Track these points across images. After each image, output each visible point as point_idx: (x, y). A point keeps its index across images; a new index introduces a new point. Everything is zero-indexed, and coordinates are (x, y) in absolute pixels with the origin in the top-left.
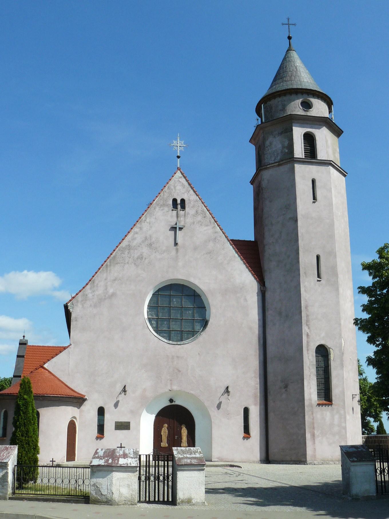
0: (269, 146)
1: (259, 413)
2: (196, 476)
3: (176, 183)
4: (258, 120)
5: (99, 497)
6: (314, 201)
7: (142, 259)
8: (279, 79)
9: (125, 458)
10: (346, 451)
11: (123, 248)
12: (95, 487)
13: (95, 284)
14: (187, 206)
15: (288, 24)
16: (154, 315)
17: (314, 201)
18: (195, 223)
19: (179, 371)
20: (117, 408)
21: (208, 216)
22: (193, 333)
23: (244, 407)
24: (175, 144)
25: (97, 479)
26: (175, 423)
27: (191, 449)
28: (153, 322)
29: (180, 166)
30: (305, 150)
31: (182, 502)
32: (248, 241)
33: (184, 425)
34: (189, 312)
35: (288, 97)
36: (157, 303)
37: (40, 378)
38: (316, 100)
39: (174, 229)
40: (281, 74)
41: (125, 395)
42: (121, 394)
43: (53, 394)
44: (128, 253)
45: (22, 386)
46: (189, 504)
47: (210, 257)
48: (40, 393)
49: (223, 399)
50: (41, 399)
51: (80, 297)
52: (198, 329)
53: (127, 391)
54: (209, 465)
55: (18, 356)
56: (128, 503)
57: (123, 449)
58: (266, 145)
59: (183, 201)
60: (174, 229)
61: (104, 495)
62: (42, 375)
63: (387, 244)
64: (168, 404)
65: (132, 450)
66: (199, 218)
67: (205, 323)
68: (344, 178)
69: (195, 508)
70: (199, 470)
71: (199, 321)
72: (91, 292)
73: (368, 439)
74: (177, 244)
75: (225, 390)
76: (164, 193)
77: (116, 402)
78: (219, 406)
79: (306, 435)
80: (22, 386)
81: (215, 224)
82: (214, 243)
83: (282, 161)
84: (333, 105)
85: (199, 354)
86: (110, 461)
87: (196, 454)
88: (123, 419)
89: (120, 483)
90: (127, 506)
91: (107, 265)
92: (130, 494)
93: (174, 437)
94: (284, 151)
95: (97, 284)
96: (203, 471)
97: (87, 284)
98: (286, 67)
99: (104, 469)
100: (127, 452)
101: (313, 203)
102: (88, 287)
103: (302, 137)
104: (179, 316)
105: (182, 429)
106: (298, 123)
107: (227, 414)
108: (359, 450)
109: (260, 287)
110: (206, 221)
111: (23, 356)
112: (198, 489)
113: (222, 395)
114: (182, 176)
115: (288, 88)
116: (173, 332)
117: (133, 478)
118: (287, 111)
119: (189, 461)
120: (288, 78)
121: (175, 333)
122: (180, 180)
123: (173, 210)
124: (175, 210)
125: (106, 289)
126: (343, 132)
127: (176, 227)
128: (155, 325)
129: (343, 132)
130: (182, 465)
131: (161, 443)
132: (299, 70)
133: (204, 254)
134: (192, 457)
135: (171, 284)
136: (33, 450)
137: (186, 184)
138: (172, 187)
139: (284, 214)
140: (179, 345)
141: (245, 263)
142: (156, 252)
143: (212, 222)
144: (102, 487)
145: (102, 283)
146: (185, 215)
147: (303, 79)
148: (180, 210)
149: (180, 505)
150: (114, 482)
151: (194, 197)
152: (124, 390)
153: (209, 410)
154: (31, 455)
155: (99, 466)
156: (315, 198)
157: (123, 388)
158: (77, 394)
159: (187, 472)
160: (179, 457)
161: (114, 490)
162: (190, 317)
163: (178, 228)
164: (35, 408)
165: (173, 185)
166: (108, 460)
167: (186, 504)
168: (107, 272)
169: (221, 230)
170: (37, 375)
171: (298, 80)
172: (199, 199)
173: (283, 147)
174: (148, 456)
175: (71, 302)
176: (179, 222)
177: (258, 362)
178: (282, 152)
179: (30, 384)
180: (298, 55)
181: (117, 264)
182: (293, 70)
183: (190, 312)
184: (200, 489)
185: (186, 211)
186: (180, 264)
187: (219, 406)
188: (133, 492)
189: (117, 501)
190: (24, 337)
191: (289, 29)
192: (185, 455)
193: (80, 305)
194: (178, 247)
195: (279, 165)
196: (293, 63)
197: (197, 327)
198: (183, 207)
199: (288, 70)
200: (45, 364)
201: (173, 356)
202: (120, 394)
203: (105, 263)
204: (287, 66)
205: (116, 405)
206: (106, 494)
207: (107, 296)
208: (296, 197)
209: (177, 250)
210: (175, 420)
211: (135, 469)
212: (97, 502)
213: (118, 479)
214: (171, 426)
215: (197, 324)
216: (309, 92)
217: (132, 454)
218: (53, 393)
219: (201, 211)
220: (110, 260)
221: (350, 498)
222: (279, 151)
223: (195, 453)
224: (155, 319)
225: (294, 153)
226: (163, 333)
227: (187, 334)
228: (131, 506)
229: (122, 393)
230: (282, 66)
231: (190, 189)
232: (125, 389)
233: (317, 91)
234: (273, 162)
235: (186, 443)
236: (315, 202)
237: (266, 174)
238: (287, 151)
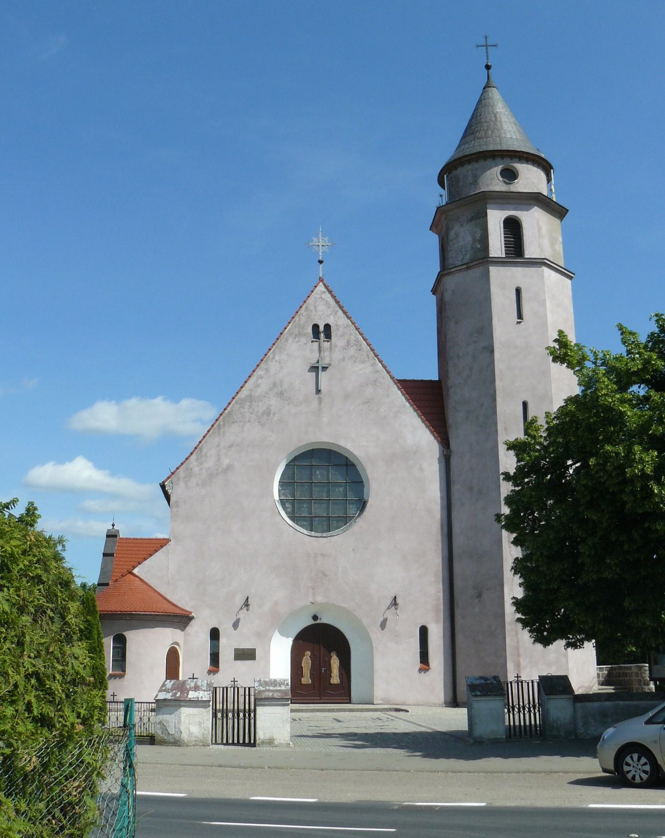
0: (454, 239)
1: (442, 634)
3: (317, 301)
4: (441, 196)
5: (165, 737)
6: (519, 320)
7: (270, 414)
8: (470, 135)
9: (196, 691)
10: (471, 683)
11: (242, 400)
13: (203, 453)
14: (333, 334)
15: (486, 46)
16: (289, 496)
17: (519, 320)
18: (346, 360)
19: (325, 575)
20: (237, 628)
21: (365, 347)
22: (345, 520)
23: (420, 626)
24: (315, 243)
26: (322, 650)
28: (287, 506)
29: (323, 275)
30: (505, 244)
31: (263, 743)
32: (427, 380)
33: (335, 652)
34: (339, 489)
35: (481, 163)
36: (293, 478)
37: (127, 589)
38: (525, 165)
39: (316, 369)
40: (473, 126)
41: (248, 610)
43: (144, 611)
44: (250, 407)
45: (85, 605)
47: (368, 409)
49: (389, 615)
50: (128, 618)
51: (181, 473)
52: (353, 514)
55: (105, 555)
57: (195, 680)
58: (450, 238)
59: (327, 327)
60: (314, 369)
62: (131, 585)
63: (535, 417)
64: (310, 622)
65: (206, 682)
66: (352, 351)
67: (362, 505)
68: (569, 281)
69: (278, 749)
71: (353, 501)
72: (198, 465)
73: (612, 670)
74: (320, 391)
75: (392, 602)
76: (299, 317)
77: (236, 621)
78: (383, 625)
79: (508, 666)
80: (85, 605)
81: (375, 360)
82: (374, 388)
83: (472, 262)
84: (553, 169)
85: (353, 550)
86: (178, 694)
87: (282, 686)
88: (246, 645)
90: (198, 747)
91: (219, 426)
93: (321, 671)
94: (475, 247)
95: (206, 453)
97: (191, 454)
98: (480, 115)
100: (199, 683)
101: (517, 324)
102: (194, 457)
103: (502, 225)
104: (325, 495)
106: (494, 203)
107: (396, 636)
108: (489, 682)
109: (442, 449)
110: (362, 355)
111: (112, 555)
113: (388, 608)
114: (326, 290)
115: (481, 150)
116: (317, 519)
117: (205, 714)
118: (480, 184)
119: (271, 694)
120: (482, 133)
121: (318, 520)
122: (323, 296)
123: (313, 341)
124: (316, 341)
125: (219, 460)
126: (568, 211)
127: (318, 367)
128: (290, 509)
129: (568, 211)
130: (262, 699)
131: (302, 679)
132: (499, 120)
133: (359, 405)
134: (275, 690)
135: (313, 449)
136: (98, 684)
137: (332, 301)
138: (312, 308)
139: (475, 342)
140: (325, 537)
141: (419, 416)
142: (289, 404)
143: (371, 357)
144: (169, 726)
145: (213, 452)
146: (331, 348)
147: (505, 134)
148: (324, 341)
150: (183, 719)
151: (343, 321)
152: (246, 604)
153: (369, 631)
155: (165, 700)
156: (520, 316)
158: (179, 610)
161: (182, 728)
162: (341, 497)
163: (320, 368)
164: (101, 632)
165: (313, 304)
166: (176, 694)
167: (268, 746)
168: (219, 435)
169: (385, 367)
171: (497, 135)
172: (351, 324)
173: (474, 240)
174: (225, 688)
175: (170, 479)
176: (322, 360)
177: (441, 559)
178: (472, 248)
179: (95, 601)
180: (501, 94)
181: (234, 423)
182: (490, 120)
183: (340, 489)
185: (332, 342)
186: (325, 420)
187: (383, 625)
190: (113, 525)
191: (487, 52)
192: (268, 688)
193: (182, 484)
194: (321, 396)
195: (468, 268)
196: (491, 108)
197: (352, 510)
198: (328, 336)
199: (483, 120)
200: (135, 569)
201: (316, 554)
202: (241, 609)
203: (217, 423)
204: (482, 113)
205: (236, 625)
207: (220, 469)
208: (492, 316)
209: (320, 401)
210: (321, 645)
211: (207, 704)
212: (163, 743)
213: (187, 715)
215: (351, 506)
216: (512, 154)
217: (205, 687)
218: (144, 610)
219: (355, 340)
220: (224, 418)
221: (472, 741)
222: (469, 247)
223: (280, 686)
224: (291, 501)
225: (490, 249)
226: (301, 520)
227: (336, 521)
228: (202, 747)
230: (475, 112)
231: (338, 309)
233: (525, 152)
234: (460, 263)
235: (338, 678)
236: (520, 322)
237: (450, 282)
238: (479, 246)
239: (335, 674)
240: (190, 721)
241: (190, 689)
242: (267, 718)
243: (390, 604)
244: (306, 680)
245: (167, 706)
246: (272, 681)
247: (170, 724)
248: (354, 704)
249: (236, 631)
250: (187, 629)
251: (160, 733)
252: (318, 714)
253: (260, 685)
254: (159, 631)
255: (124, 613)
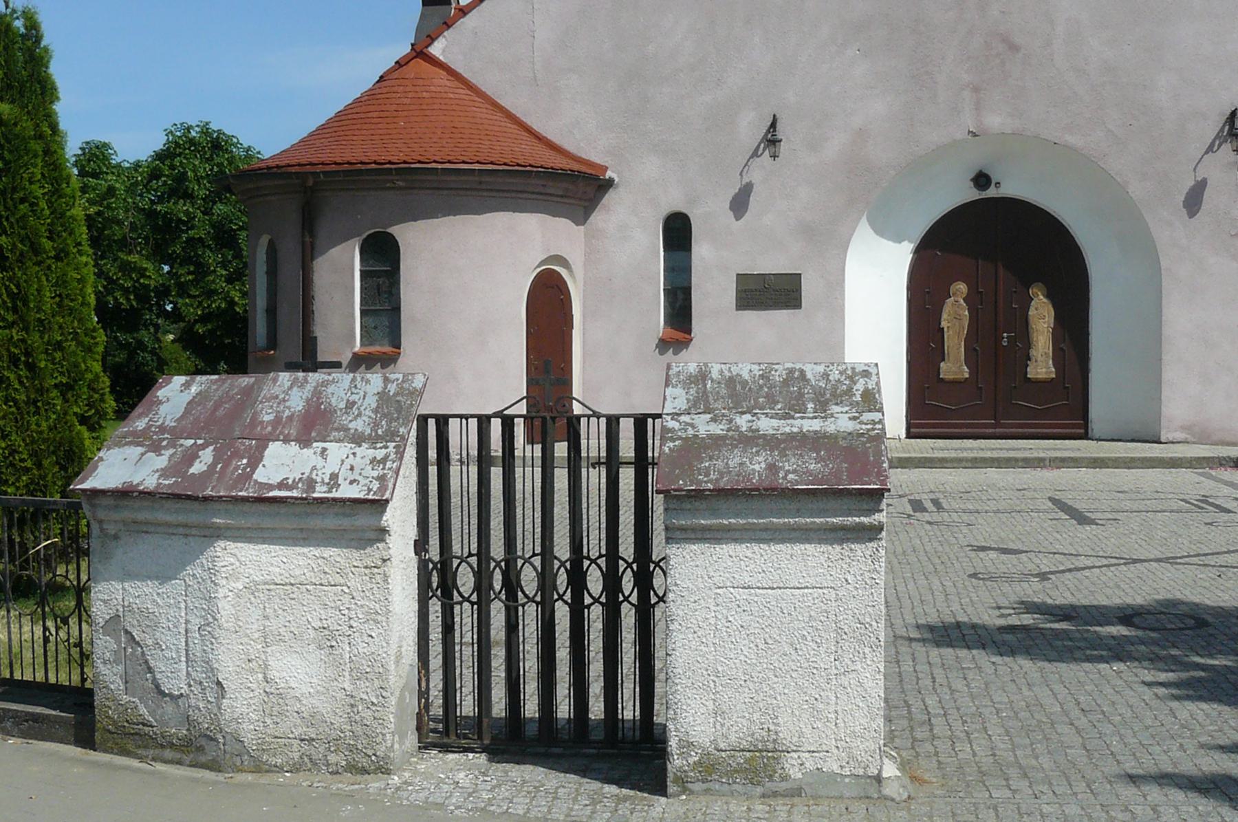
2: (811, 581)
5: (143, 710)
12: (118, 642)
19: (1014, 48)
20: (741, 218)
25: (126, 585)
27: (809, 375)
31: (709, 767)
37: (406, 101)
41: (774, 156)
42: (758, 157)
43: (450, 162)
46: (759, 790)
48: (394, 159)
50: (401, 183)
53: (780, 141)
54: (1139, 459)
56: (332, 758)
61: (171, 696)
62: (418, 89)
64: (970, 194)
70: (840, 534)
75: (1222, 130)
78: (1194, 201)
87: (835, 409)
89: (266, 618)
92: (340, 695)
96: (874, 544)
99: (162, 516)
105: (1033, 303)
112: (828, 681)
113: (1210, 149)
117: (354, 582)
119: (757, 465)
131: (942, 364)
134: (791, 437)
149: (692, 792)
150: (225, 608)
152: (771, 140)
154: (44, 424)
157: (768, 131)
159: (742, 550)
160: (691, 432)
161: (228, 666)
166: (191, 457)
170: (395, 89)
174: (496, 426)
184: (844, 680)
187: (1194, 201)
188: (361, 684)
189: (249, 738)
192: (743, 421)
200: (436, 43)
202: (755, 154)
205: (740, 204)
206: (185, 689)
213: (252, 589)
214: (981, 290)
229: (764, 150)
232: (775, 131)
235: (1051, 362)
239: (1041, 351)
240: (274, 624)
241: (278, 431)
242: (737, 620)
243: (1217, 137)
244: (954, 367)
245: (141, 528)
246: (778, 375)
247: (166, 638)
248: (1098, 440)
249: (739, 222)
250: (592, 218)
251: (117, 684)
252: (992, 473)
253: (702, 403)
254: (500, 222)
255: (388, 166)
